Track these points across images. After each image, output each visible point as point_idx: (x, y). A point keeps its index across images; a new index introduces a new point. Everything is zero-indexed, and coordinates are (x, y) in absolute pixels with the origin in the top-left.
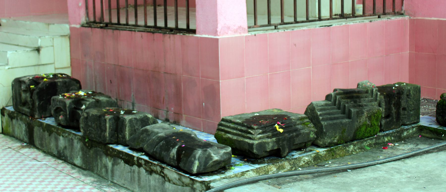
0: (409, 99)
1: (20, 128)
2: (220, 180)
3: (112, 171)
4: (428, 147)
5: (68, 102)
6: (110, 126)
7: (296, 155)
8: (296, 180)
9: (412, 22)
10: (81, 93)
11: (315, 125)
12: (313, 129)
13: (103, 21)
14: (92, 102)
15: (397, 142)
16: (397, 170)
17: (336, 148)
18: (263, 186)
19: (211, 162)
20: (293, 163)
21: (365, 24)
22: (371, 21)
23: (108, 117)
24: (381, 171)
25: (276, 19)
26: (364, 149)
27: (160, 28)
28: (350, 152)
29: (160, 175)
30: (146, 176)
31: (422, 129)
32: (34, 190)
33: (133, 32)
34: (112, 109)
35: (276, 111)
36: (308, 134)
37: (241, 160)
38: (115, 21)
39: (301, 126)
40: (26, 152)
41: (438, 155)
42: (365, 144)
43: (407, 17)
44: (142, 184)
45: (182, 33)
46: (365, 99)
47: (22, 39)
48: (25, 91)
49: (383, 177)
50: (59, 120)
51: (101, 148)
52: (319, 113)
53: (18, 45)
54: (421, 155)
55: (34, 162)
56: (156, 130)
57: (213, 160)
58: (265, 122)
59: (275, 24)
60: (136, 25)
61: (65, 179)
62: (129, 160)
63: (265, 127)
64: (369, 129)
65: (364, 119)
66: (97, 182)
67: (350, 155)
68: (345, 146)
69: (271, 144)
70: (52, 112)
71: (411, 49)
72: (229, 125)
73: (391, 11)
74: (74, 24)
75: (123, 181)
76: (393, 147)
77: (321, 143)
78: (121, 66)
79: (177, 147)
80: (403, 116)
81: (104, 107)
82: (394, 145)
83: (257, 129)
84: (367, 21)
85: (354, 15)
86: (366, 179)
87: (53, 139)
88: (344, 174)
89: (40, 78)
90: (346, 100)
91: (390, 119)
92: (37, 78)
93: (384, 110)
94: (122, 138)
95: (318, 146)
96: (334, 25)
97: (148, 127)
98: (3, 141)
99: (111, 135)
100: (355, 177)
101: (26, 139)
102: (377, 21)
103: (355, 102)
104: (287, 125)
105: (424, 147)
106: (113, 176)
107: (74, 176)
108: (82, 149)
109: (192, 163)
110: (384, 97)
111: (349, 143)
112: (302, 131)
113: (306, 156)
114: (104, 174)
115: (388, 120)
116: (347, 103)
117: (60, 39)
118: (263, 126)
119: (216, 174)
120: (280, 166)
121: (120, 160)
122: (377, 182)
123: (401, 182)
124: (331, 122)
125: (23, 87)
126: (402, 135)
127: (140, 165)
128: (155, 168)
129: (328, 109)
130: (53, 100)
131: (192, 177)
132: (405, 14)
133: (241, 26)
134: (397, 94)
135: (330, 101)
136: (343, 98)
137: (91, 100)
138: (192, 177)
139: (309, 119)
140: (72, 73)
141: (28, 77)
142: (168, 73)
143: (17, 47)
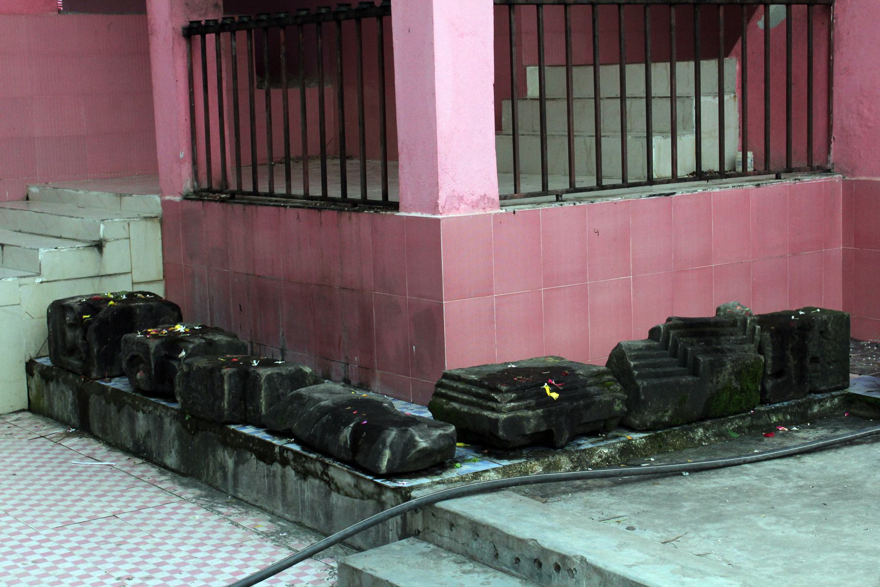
0: (825, 341)
1: (63, 399)
2: (430, 486)
3: (235, 476)
4: (852, 433)
5: (153, 344)
6: (230, 390)
7: (586, 444)
8: (579, 489)
9: (847, 185)
10: (180, 328)
13: (227, 187)
14: (199, 345)
15: (796, 425)
16: (781, 475)
17: (666, 433)
18: (510, 497)
19: (413, 451)
20: (578, 458)
21: (746, 194)
22: (758, 185)
23: (226, 371)
24: (748, 475)
25: (558, 183)
27: (334, 200)
29: (321, 479)
30: (296, 483)
31: (852, 400)
32: (102, 584)
33: (282, 209)
34: (236, 358)
35: (551, 360)
36: (611, 404)
37: (476, 452)
38: (248, 187)
39: (597, 388)
40: (73, 445)
41: (872, 448)
43: (837, 177)
44: (290, 497)
45: (373, 209)
46: (728, 338)
47: (70, 225)
48: (73, 326)
49: (749, 485)
50: (137, 381)
51: (215, 432)
52: (632, 363)
53: (60, 237)
54: (837, 448)
55: (89, 462)
56: (316, 395)
57: (418, 448)
58: (524, 380)
59: (556, 191)
60: (288, 196)
61: (146, 491)
62: (265, 453)
63: (523, 389)
64: (737, 397)
65: (727, 377)
66: (206, 497)
67: (696, 447)
69: (532, 419)
70: (124, 365)
71: (845, 242)
72: (455, 385)
73: (804, 164)
74: (169, 194)
75: (254, 495)
76: (787, 433)
77: (637, 422)
78: (259, 276)
79: (352, 425)
80: (812, 374)
81: (223, 355)
82: (790, 430)
84: (750, 186)
86: (714, 489)
87: (125, 419)
88: (675, 480)
89: (101, 299)
91: (784, 379)
92: (96, 299)
93: (770, 361)
94: (254, 411)
96: (679, 194)
97: (303, 390)
98: (30, 425)
99: (233, 407)
100: (694, 485)
101: (74, 421)
102: (772, 186)
103: (708, 343)
105: (845, 434)
106: (235, 486)
107: (163, 486)
108: (179, 435)
109: (380, 454)
110: (771, 335)
111: (694, 425)
112: (597, 398)
113: (605, 446)
114: (219, 482)
115: (779, 380)
116: (692, 345)
117: (143, 224)
119: (425, 476)
120: (550, 464)
121: (248, 455)
122: (735, 495)
123: (781, 495)
124: (655, 381)
125: (69, 318)
126: (809, 412)
127: (284, 463)
128: (312, 467)
129: (652, 357)
130: (126, 340)
131: (379, 481)
132: (835, 170)
134: (799, 328)
135: (658, 341)
137: (197, 341)
138: (379, 481)
139: (615, 376)
140: (166, 292)
141: (78, 299)
142: (347, 289)
143: (59, 240)
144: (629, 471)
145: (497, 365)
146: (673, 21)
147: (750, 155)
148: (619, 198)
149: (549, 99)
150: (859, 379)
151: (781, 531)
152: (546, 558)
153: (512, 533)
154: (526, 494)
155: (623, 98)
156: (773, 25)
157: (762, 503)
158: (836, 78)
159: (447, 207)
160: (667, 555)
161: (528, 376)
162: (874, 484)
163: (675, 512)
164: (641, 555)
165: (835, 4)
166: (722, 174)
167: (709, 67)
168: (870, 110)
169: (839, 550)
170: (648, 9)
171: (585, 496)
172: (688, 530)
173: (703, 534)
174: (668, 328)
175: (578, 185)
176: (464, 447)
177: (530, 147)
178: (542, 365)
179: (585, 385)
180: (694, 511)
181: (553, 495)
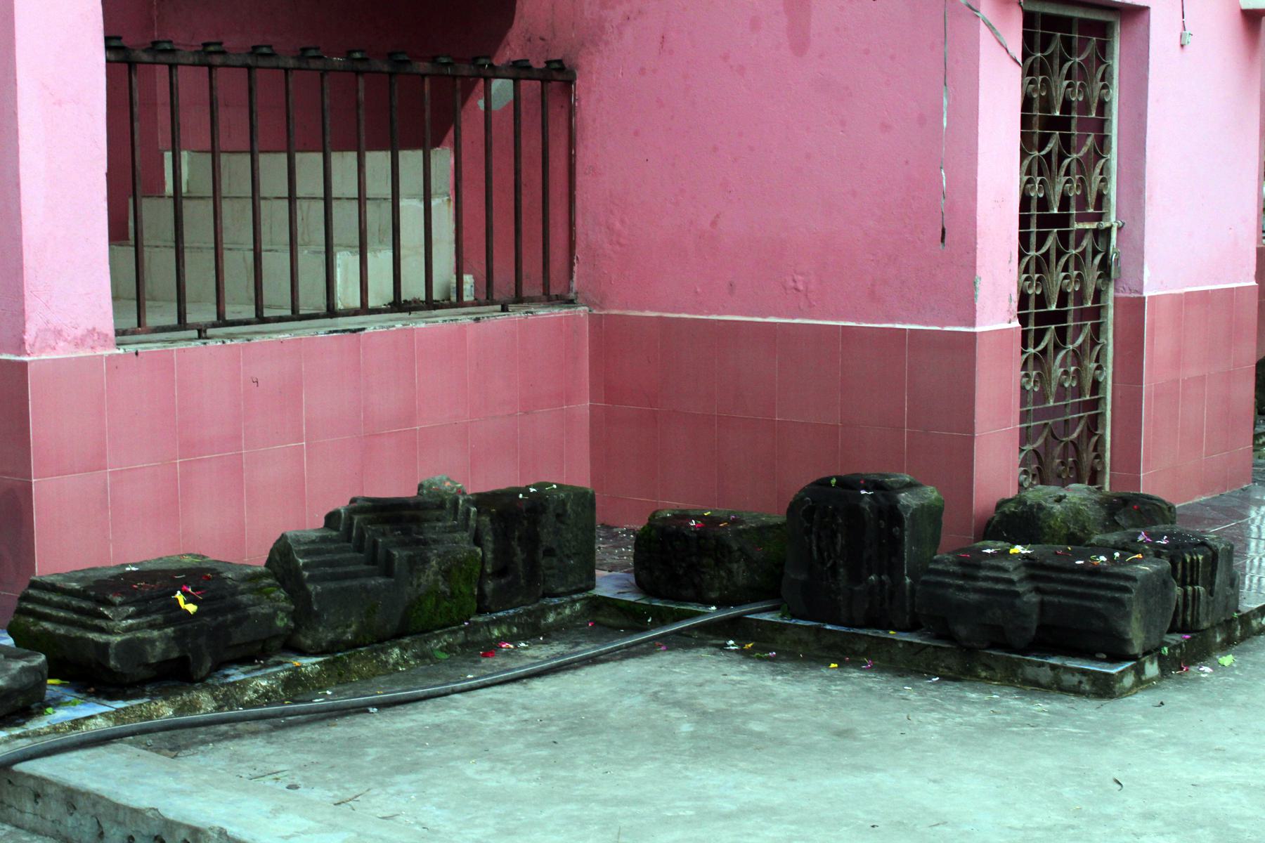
0: (563, 527)
4: (595, 648)
7: (236, 675)
8: (225, 737)
9: (596, 321)
11: (292, 595)
12: (284, 604)
15: (524, 640)
18: (124, 751)
20: (225, 695)
21: (463, 328)
22: (477, 320)
24: (456, 708)
25: (202, 313)
26: (430, 658)
28: (390, 667)
31: (599, 604)
35: (187, 559)
36: (271, 617)
37: (78, 691)
39: (251, 597)
41: (1106, 762)
42: (435, 644)
43: (582, 310)
52: (301, 561)
54: (576, 668)
58: (148, 589)
59: (198, 324)
64: (446, 604)
65: (432, 577)
67: (390, 674)
68: (376, 651)
69: (159, 642)
72: (47, 597)
73: (538, 292)
76: (512, 650)
77: (309, 642)
80: (548, 572)
83: (122, 604)
84: (466, 320)
85: (454, 301)
88: (359, 719)
90: (380, 527)
91: (510, 578)
93: (489, 556)
95: (303, 653)
96: (370, 330)
102: (495, 319)
103: (406, 532)
104: (209, 595)
105: (587, 649)
111: (388, 643)
112: (252, 611)
113: (263, 677)
116: (384, 534)
118: (139, 596)
120: (185, 703)
122: (438, 735)
123: (499, 734)
124: (332, 585)
129: (329, 552)
132: (579, 301)
133: (94, 329)
134: (527, 511)
135: (337, 529)
136: (371, 522)
139: (277, 579)
144: (294, 710)
145: (110, 568)
146: (361, 95)
147: (468, 279)
148: (285, 334)
149: (265, 198)
150: (609, 577)
151: (501, 779)
152: (171, 834)
153: (123, 801)
154: (147, 747)
155: (292, 198)
156: (496, 105)
157: (474, 744)
158: (580, 179)
159: (37, 345)
160: (340, 820)
161: (154, 582)
162: (620, 712)
163: (357, 761)
164: (304, 821)
165: (577, 82)
166: (430, 304)
167: (411, 160)
168: (622, 222)
169: (567, 801)
170: (326, 77)
171: (232, 746)
172: (371, 784)
173: (391, 790)
174: (352, 512)
175: (228, 317)
176: (60, 685)
177: (160, 262)
178: (174, 566)
179: (234, 592)
180: (381, 759)
181: (186, 747)
